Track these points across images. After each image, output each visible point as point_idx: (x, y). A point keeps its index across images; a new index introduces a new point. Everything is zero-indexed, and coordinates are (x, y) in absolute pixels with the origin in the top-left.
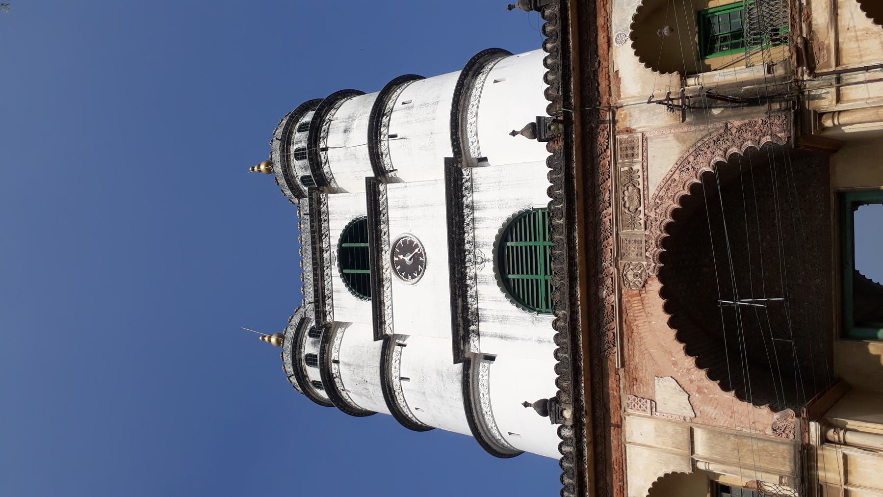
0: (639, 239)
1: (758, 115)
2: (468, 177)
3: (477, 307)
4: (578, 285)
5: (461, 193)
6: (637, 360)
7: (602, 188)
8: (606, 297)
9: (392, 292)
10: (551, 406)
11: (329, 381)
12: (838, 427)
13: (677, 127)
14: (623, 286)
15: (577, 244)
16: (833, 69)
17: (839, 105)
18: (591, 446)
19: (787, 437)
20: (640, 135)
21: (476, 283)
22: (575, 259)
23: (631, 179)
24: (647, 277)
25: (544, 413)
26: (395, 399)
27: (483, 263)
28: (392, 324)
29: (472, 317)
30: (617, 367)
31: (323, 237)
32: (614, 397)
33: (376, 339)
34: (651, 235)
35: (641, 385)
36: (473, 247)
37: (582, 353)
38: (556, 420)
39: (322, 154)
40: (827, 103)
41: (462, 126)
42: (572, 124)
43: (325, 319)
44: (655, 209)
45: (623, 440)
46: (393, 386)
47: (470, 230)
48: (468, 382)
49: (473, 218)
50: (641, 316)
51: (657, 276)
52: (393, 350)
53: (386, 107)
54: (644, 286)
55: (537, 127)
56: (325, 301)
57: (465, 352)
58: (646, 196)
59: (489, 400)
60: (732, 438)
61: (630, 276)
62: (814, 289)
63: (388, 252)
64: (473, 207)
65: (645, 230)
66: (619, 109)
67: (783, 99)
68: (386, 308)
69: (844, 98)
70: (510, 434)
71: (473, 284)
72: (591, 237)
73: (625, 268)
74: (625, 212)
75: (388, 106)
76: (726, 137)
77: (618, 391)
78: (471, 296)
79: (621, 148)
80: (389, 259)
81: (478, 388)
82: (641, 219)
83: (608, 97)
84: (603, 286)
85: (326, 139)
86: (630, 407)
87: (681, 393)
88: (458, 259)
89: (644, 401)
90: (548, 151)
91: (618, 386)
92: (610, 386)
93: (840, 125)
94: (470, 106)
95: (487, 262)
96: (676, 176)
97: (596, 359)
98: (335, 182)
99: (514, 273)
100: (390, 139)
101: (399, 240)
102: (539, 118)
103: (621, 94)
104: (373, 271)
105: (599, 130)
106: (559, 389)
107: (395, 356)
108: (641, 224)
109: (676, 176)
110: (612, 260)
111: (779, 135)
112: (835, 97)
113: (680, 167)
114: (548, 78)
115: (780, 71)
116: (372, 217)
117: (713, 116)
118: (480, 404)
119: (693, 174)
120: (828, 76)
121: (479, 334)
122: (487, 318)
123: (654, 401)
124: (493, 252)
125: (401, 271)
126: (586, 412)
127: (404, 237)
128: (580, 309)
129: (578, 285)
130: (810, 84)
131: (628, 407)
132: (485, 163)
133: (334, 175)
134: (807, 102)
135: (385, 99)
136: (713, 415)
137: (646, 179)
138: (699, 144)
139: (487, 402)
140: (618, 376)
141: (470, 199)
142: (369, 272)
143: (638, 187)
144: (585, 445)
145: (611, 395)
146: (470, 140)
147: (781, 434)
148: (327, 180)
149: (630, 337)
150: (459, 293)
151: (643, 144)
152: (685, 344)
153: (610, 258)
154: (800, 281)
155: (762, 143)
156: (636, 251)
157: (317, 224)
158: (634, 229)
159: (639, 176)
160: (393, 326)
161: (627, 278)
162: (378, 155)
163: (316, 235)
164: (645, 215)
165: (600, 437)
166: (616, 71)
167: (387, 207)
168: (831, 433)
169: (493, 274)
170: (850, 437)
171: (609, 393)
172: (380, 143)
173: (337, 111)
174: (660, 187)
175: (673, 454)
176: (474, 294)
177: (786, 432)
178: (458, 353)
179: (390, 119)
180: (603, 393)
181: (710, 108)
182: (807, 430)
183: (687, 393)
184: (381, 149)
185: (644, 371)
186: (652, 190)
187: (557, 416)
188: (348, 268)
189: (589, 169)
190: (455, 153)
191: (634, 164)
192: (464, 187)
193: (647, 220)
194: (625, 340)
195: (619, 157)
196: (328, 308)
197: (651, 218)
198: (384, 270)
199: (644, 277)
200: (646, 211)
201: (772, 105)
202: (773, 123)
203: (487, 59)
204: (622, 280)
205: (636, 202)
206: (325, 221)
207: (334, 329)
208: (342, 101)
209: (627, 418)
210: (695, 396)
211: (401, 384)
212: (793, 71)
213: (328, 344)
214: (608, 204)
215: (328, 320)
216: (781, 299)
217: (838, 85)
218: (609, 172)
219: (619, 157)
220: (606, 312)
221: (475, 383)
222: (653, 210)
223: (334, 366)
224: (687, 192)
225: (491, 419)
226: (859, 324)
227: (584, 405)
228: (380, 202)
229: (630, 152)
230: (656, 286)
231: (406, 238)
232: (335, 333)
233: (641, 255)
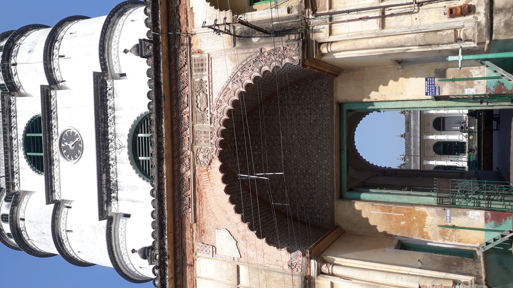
0: (207, 130)
1: (281, 42)
2: (111, 87)
3: (117, 180)
4: (165, 164)
5: (106, 98)
6: (204, 217)
7: (182, 93)
8: (185, 172)
9: (60, 169)
10: (148, 253)
11: (17, 233)
12: (329, 263)
13: (230, 50)
14: (196, 164)
15: (164, 133)
16: (327, 11)
17: (330, 37)
18: (173, 281)
19: (297, 271)
20: (207, 56)
21: (116, 162)
22: (162, 144)
23: (201, 87)
24: (212, 158)
25: (144, 257)
26: (63, 245)
27: (121, 149)
28: (59, 193)
29: (113, 187)
30: (191, 222)
31: (13, 128)
32: (189, 244)
33: (48, 202)
34: (214, 127)
35: (207, 235)
36: (114, 137)
37: (166, 214)
38: (151, 262)
39: (13, 68)
40: (323, 35)
41: (108, 50)
42: (160, 44)
43: (13, 189)
44: (217, 109)
45: (194, 275)
46: (61, 237)
47: (112, 124)
48: (111, 233)
49: (114, 116)
50: (208, 185)
51: (218, 157)
52: (62, 210)
53: (58, 35)
54: (209, 164)
55: (140, 47)
56: (14, 175)
57: (108, 212)
58: (211, 100)
59: (126, 245)
60: (264, 272)
61: (201, 157)
62: (324, 166)
63: (57, 140)
64: (114, 109)
65: (211, 124)
66: (194, 36)
67: (296, 32)
68: (55, 181)
69: (334, 32)
70: (141, 268)
71: (114, 163)
72: (175, 128)
73: (198, 151)
74: (198, 111)
75: (60, 35)
76: (261, 59)
77: (192, 240)
78: (113, 172)
79: (195, 65)
80: (58, 146)
81: (118, 237)
82: (208, 116)
83: (186, 26)
84: (183, 165)
85: (16, 57)
86: (199, 251)
87: (232, 240)
88: (103, 146)
89: (208, 247)
90: (148, 65)
91: (192, 236)
92: (186, 236)
93: (332, 52)
94: (114, 37)
95: (124, 148)
96: (230, 86)
97: (178, 217)
98: (23, 88)
99: (143, 156)
100: (59, 58)
101: (65, 132)
102: (140, 40)
103: (195, 25)
104: (46, 154)
105: (180, 50)
106: (154, 240)
107: (63, 215)
108: (208, 120)
109: (230, 86)
110: (189, 146)
111: (294, 58)
112: (328, 31)
113: (232, 79)
114: (147, 11)
115: (295, 12)
116: (45, 114)
117: (253, 43)
118: (120, 248)
119: (240, 85)
120: (325, 16)
121: (118, 199)
122: (123, 188)
123: (214, 247)
124: (128, 141)
125: (66, 154)
126: (169, 256)
127: (69, 129)
128: (165, 181)
129: (165, 164)
130: (314, 22)
131: (198, 251)
132: (125, 77)
133: (21, 84)
134: (311, 34)
135: (59, 30)
136: (252, 256)
137: (211, 87)
138: (244, 64)
139: (124, 246)
140: (192, 229)
141: (112, 102)
142: (42, 154)
143: (206, 93)
144: (167, 280)
145: (187, 243)
146: (114, 61)
147: (294, 269)
148: (17, 87)
149: (201, 201)
150: (103, 170)
151: (209, 62)
152: (235, 205)
153: (188, 144)
154: (315, 161)
155: (283, 64)
156: (205, 139)
157: (8, 119)
158: (203, 124)
159: (207, 85)
160: (61, 194)
161: (199, 158)
162: (51, 70)
163: (7, 127)
164: (210, 113)
165: (179, 274)
166: (191, 8)
167: (57, 107)
168: (324, 268)
169: (127, 156)
170: (336, 270)
171: (186, 242)
172: (53, 61)
173: (26, 38)
174: (220, 93)
175: (226, 284)
176: (114, 171)
177: (297, 267)
178: (103, 213)
179: (60, 44)
180: (182, 242)
181: (251, 37)
182: (309, 266)
183: (236, 240)
184: (53, 65)
185: (209, 225)
186: (215, 96)
187: (152, 260)
188: (30, 152)
189: (173, 78)
190: (102, 69)
191: (203, 76)
192: (108, 94)
193: (212, 117)
194: (197, 203)
195: (194, 71)
196: (16, 181)
197: (214, 116)
198: (54, 154)
199: (209, 158)
200: (211, 111)
201: (290, 36)
202: (290, 49)
203: (130, 6)
204: (195, 160)
205: (205, 104)
206: (14, 117)
207: (22, 196)
208: (31, 32)
209: (197, 259)
210: (241, 242)
211: (67, 234)
212: (303, 12)
213: (17, 207)
214: (186, 105)
215: (15, 190)
216: (282, 173)
217: (330, 23)
218: (187, 82)
219: (194, 71)
220: (185, 183)
221: (116, 233)
222: (216, 109)
223: (21, 222)
224: (236, 98)
225: (127, 258)
226: (351, 190)
227: (167, 252)
228: (52, 103)
229: (201, 67)
230: (217, 164)
231: (70, 130)
232: (22, 198)
233: (208, 142)
